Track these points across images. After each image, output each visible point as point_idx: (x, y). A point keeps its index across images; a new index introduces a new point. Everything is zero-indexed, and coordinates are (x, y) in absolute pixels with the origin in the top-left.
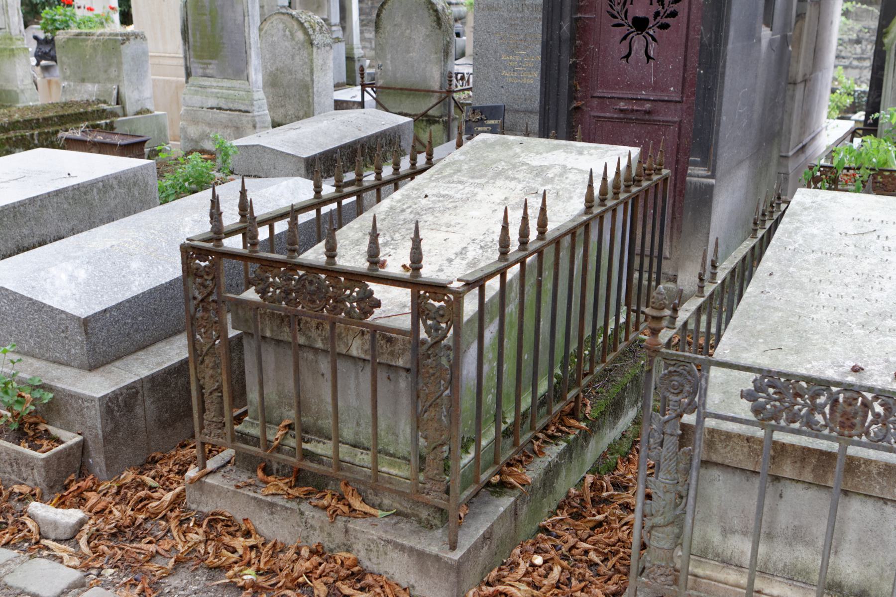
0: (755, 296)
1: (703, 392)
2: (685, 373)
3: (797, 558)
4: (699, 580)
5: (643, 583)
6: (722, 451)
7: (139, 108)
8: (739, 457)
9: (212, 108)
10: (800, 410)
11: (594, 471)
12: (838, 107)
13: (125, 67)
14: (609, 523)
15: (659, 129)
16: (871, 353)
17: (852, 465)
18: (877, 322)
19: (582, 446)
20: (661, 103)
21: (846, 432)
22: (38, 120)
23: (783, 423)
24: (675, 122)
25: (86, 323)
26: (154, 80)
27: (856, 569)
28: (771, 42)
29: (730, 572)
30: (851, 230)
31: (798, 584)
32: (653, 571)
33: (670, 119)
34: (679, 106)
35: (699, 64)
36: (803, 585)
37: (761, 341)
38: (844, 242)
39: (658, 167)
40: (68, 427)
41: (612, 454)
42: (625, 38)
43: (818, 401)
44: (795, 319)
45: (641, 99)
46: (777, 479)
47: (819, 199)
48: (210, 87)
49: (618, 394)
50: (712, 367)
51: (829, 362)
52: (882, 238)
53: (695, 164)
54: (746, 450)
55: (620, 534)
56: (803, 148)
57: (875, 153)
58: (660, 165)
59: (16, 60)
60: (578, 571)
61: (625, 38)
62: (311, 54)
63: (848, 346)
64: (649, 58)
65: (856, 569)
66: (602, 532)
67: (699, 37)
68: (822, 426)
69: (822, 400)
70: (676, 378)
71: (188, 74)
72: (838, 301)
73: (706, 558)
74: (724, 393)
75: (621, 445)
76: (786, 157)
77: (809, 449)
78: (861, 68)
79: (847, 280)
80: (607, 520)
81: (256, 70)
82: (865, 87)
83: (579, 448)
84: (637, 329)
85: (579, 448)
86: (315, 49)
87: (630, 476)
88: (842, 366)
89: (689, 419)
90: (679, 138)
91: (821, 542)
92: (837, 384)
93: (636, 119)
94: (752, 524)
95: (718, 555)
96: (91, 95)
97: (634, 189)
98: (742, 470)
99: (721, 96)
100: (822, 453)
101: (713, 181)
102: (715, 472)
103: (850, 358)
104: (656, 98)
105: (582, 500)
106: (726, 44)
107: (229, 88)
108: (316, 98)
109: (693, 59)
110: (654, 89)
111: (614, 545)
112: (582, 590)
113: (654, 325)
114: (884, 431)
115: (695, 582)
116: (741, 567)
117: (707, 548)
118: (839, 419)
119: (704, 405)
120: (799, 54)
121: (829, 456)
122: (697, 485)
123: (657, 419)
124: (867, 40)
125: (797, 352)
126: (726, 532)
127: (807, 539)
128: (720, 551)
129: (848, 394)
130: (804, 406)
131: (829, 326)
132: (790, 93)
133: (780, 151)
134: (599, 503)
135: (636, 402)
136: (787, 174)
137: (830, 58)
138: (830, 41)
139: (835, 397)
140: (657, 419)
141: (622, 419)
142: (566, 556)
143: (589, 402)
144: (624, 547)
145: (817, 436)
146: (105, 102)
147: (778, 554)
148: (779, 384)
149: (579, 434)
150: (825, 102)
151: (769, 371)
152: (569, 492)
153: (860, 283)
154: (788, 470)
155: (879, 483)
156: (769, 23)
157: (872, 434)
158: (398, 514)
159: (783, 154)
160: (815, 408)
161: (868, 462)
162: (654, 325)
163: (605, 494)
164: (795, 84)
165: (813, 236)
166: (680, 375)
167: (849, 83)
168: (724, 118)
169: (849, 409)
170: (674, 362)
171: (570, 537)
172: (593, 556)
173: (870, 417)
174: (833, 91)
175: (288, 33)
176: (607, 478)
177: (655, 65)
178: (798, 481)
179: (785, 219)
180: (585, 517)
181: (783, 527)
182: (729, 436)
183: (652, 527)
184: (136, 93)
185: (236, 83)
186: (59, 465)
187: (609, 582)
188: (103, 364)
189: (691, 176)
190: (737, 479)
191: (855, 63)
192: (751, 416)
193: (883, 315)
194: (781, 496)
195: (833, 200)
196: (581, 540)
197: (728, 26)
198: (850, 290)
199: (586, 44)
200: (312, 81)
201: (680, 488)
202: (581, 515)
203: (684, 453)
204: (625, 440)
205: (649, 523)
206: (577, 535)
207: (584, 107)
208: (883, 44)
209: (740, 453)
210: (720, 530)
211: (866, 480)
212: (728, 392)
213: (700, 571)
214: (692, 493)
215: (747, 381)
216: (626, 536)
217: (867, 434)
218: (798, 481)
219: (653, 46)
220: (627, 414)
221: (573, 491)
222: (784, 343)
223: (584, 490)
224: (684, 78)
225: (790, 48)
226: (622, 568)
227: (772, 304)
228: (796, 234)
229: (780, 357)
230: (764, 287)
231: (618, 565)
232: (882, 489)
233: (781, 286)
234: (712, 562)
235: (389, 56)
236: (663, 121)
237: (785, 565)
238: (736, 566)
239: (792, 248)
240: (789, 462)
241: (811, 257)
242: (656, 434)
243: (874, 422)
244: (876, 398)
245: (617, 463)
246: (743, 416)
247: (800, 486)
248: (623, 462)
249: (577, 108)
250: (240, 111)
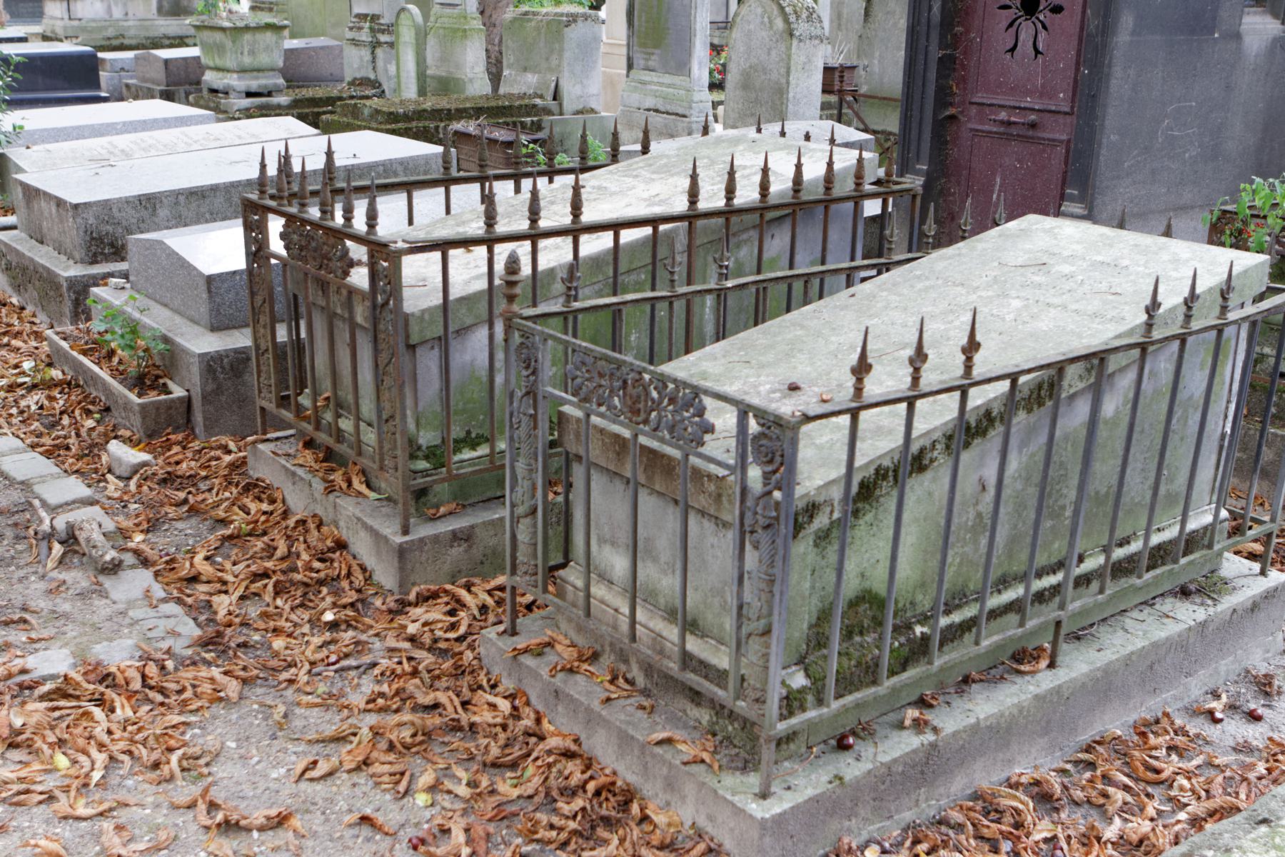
7: (581, 107)
9: (649, 110)
13: (567, 55)
15: (1044, 151)
22: (449, 110)
24: (1062, 142)
25: (210, 279)
26: (604, 72)
33: (1057, 136)
34: (1069, 119)
40: (181, 385)
42: (1011, 25)
45: (1025, 109)
48: (650, 83)
59: (469, 43)
61: (1011, 25)
62: (789, 48)
64: (1037, 52)
71: (630, 66)
81: (700, 63)
86: (795, 42)
90: (1066, 163)
93: (1018, 135)
96: (529, 88)
107: (669, 86)
108: (790, 106)
110: (1041, 96)
146: (541, 97)
158: (389, 499)
175: (766, 20)
184: (578, 87)
185: (677, 80)
186: (158, 415)
188: (227, 328)
199: (967, 31)
200: (788, 83)
207: (960, 117)
218: (448, 413)
219: (1042, 35)
235: (877, 54)
249: (953, 118)
250: (677, 114)
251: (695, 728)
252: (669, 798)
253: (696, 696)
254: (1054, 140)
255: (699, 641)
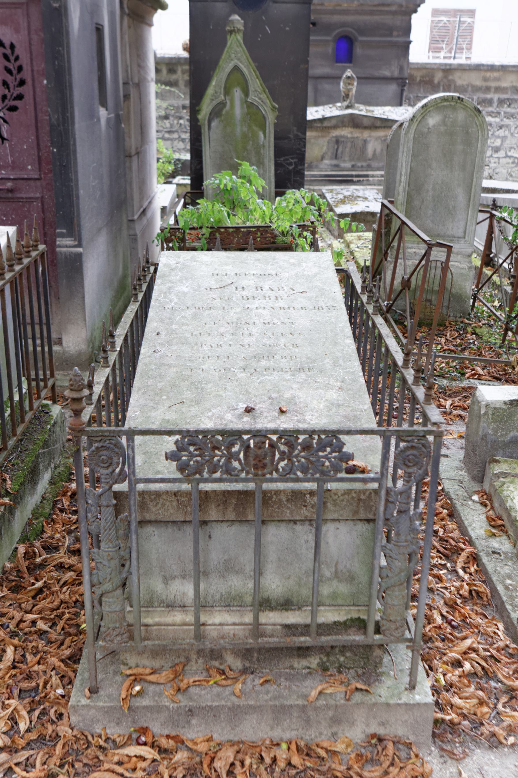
0: (150, 356)
1: (131, 461)
2: (112, 446)
3: (230, 587)
4: (149, 628)
5: (101, 647)
6: (154, 509)
8: (169, 511)
10: (219, 461)
11: (24, 539)
12: (163, 174)
14: (49, 589)
15: (24, 206)
16: (256, 393)
17: (267, 498)
18: (254, 364)
19: (9, 521)
20: (22, 182)
21: (260, 473)
23: (206, 475)
24: (37, 198)
27: (279, 583)
28: (108, 120)
29: (176, 613)
30: (213, 283)
31: (235, 608)
32: (109, 633)
33: (32, 195)
34: (38, 183)
35: (52, 143)
36: (239, 608)
37: (164, 397)
38: (210, 296)
39: (35, 244)
41: (37, 519)
43: (233, 450)
44: (188, 372)
46: (204, 523)
47: (181, 260)
49: (33, 462)
50: (136, 437)
51: (225, 407)
52: (240, 289)
53: (62, 235)
54: (175, 504)
55: (62, 596)
56: (144, 212)
57: (211, 213)
58: (36, 241)
60: (30, 645)
63: (237, 390)
65: (279, 583)
66: (44, 599)
67: (47, 118)
68: (239, 471)
69: (236, 448)
70: (104, 452)
72: (219, 349)
73: (153, 607)
74: (144, 454)
75: (43, 508)
76: (133, 221)
77: (229, 492)
78: (172, 140)
79: (222, 330)
80: (46, 585)
82: (187, 157)
83: (7, 523)
84: (39, 397)
85: (7, 523)
87: (58, 536)
88: (236, 409)
89: (122, 487)
90: (43, 212)
91: (249, 567)
92: (247, 432)
94: (190, 567)
95: (163, 602)
97: (17, 268)
98: (173, 522)
99: (76, 172)
100: (239, 492)
101: (80, 250)
102: (149, 529)
103: (241, 401)
104: (16, 177)
105: (19, 571)
106: (73, 123)
109: (45, 139)
111: (58, 608)
112: (39, 663)
113: (76, 406)
114: (290, 465)
115: (146, 631)
116: (184, 606)
117: (152, 598)
118: (253, 462)
119: (134, 472)
120: (130, 131)
121: (246, 493)
122: (138, 546)
123: (92, 494)
124: (173, 116)
125: (198, 403)
126: (166, 580)
127: (236, 569)
128: (164, 597)
129: (257, 439)
130: (221, 457)
131: (217, 374)
132: (127, 164)
133: (127, 216)
134: (34, 570)
135: (49, 464)
136: (135, 235)
137: (153, 133)
138: (150, 118)
139: (247, 444)
140: (92, 494)
141: (40, 483)
142: (15, 632)
143: (7, 476)
144: (68, 607)
145: (236, 481)
147: (215, 587)
148: (198, 441)
149: (5, 510)
150: (154, 168)
151: (188, 431)
152: (4, 567)
153: (232, 331)
154: (213, 514)
155: (289, 508)
156: (103, 103)
157: (281, 470)
159: (130, 218)
160: (231, 456)
161: (278, 492)
162: (76, 406)
163: (38, 560)
164: (130, 156)
165: (185, 294)
166: (108, 449)
167: (169, 152)
168: (81, 192)
169: (259, 452)
170: (100, 438)
171: (15, 612)
172: (41, 625)
173: (277, 456)
174: (158, 160)
176: (37, 544)
177: (10, 146)
178: (222, 521)
179: (158, 281)
180: (26, 588)
181: (215, 563)
182: (158, 494)
183: (102, 595)
187: (63, 647)
189: (60, 246)
190: (170, 530)
191: (167, 136)
192: (178, 475)
193: (257, 357)
194: (210, 537)
195: (193, 259)
196: (27, 612)
197: (72, 107)
198: (226, 339)
201: (122, 553)
202: (21, 586)
203: (121, 520)
204: (45, 502)
205: (98, 592)
206: (21, 608)
208: (197, 120)
209: (170, 507)
210: (161, 579)
211: (278, 508)
212: (147, 452)
213: (149, 620)
214: (134, 555)
215: (169, 443)
216: (67, 597)
217: (277, 470)
218: (222, 521)
220: (43, 478)
221: (8, 565)
222: (184, 397)
223: (18, 561)
224: (39, 158)
225: (123, 126)
226: (71, 630)
227: (165, 361)
228: (170, 293)
229: (184, 410)
230: (155, 346)
231: (67, 627)
232: (291, 513)
233: (169, 343)
234: (159, 609)
236: (26, 198)
237: (222, 595)
238: (180, 606)
239: (170, 307)
240: (213, 506)
241: (188, 313)
242: (93, 508)
243: (281, 459)
244: (280, 438)
245: (43, 526)
246: (172, 476)
247: (225, 525)
248: (48, 524)
251: (310, 673)
252: (335, 729)
253: (303, 651)
254: (30, 198)
255: (297, 613)
